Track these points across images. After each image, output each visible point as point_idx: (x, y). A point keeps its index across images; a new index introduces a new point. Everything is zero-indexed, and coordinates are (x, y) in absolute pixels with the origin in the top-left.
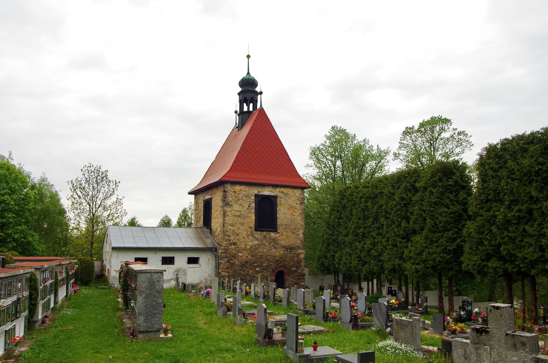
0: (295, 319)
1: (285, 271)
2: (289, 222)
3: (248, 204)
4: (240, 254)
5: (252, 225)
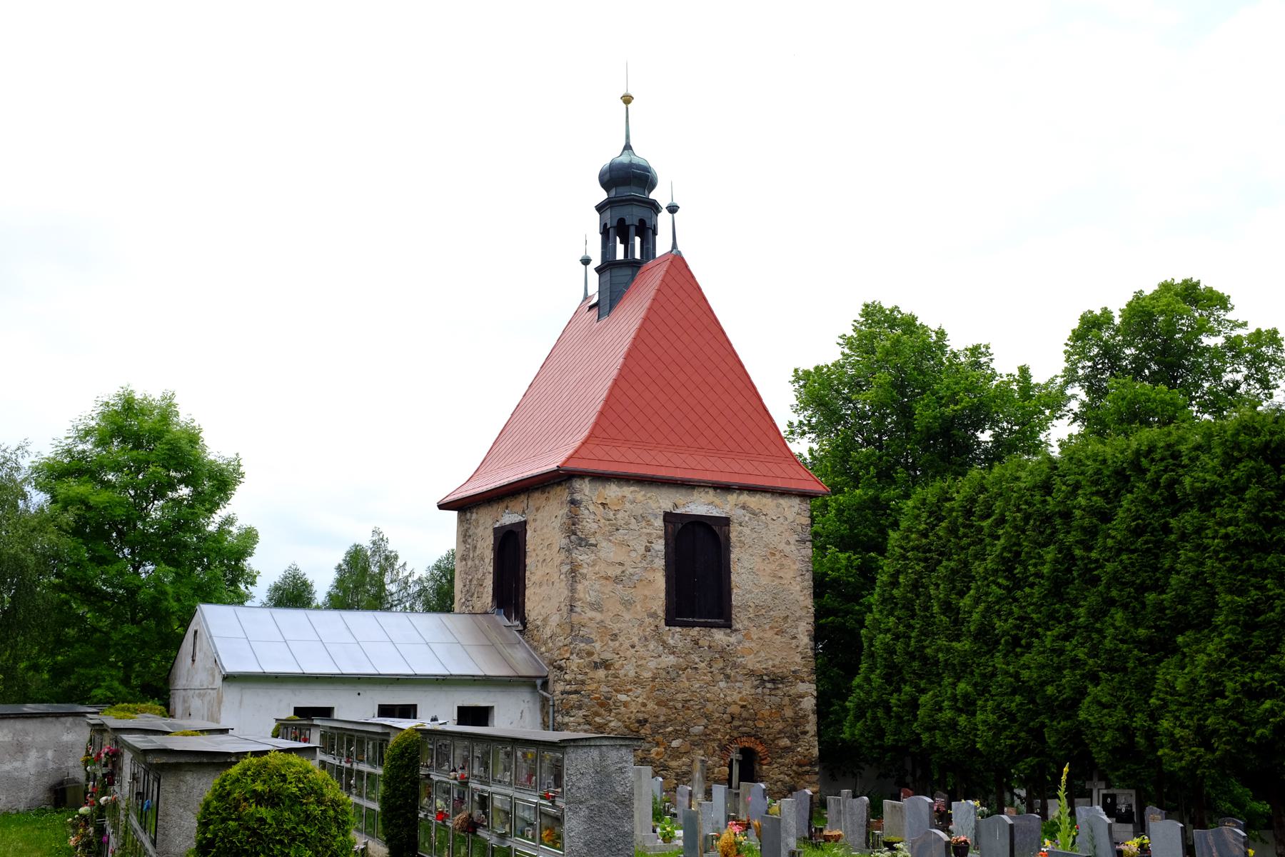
1: (759, 748)
2: (768, 597)
4: (623, 697)
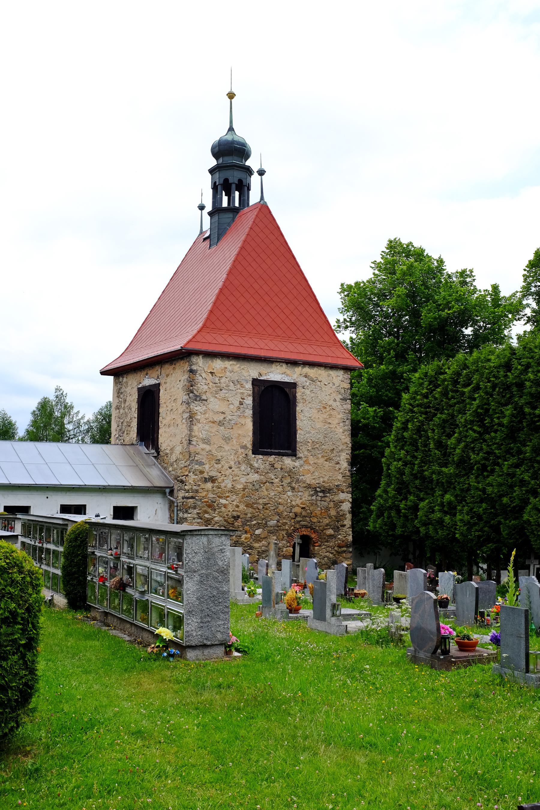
0: (523, 615)
2: (321, 436)
3: (239, 399)
4: (223, 501)
5: (248, 440)
